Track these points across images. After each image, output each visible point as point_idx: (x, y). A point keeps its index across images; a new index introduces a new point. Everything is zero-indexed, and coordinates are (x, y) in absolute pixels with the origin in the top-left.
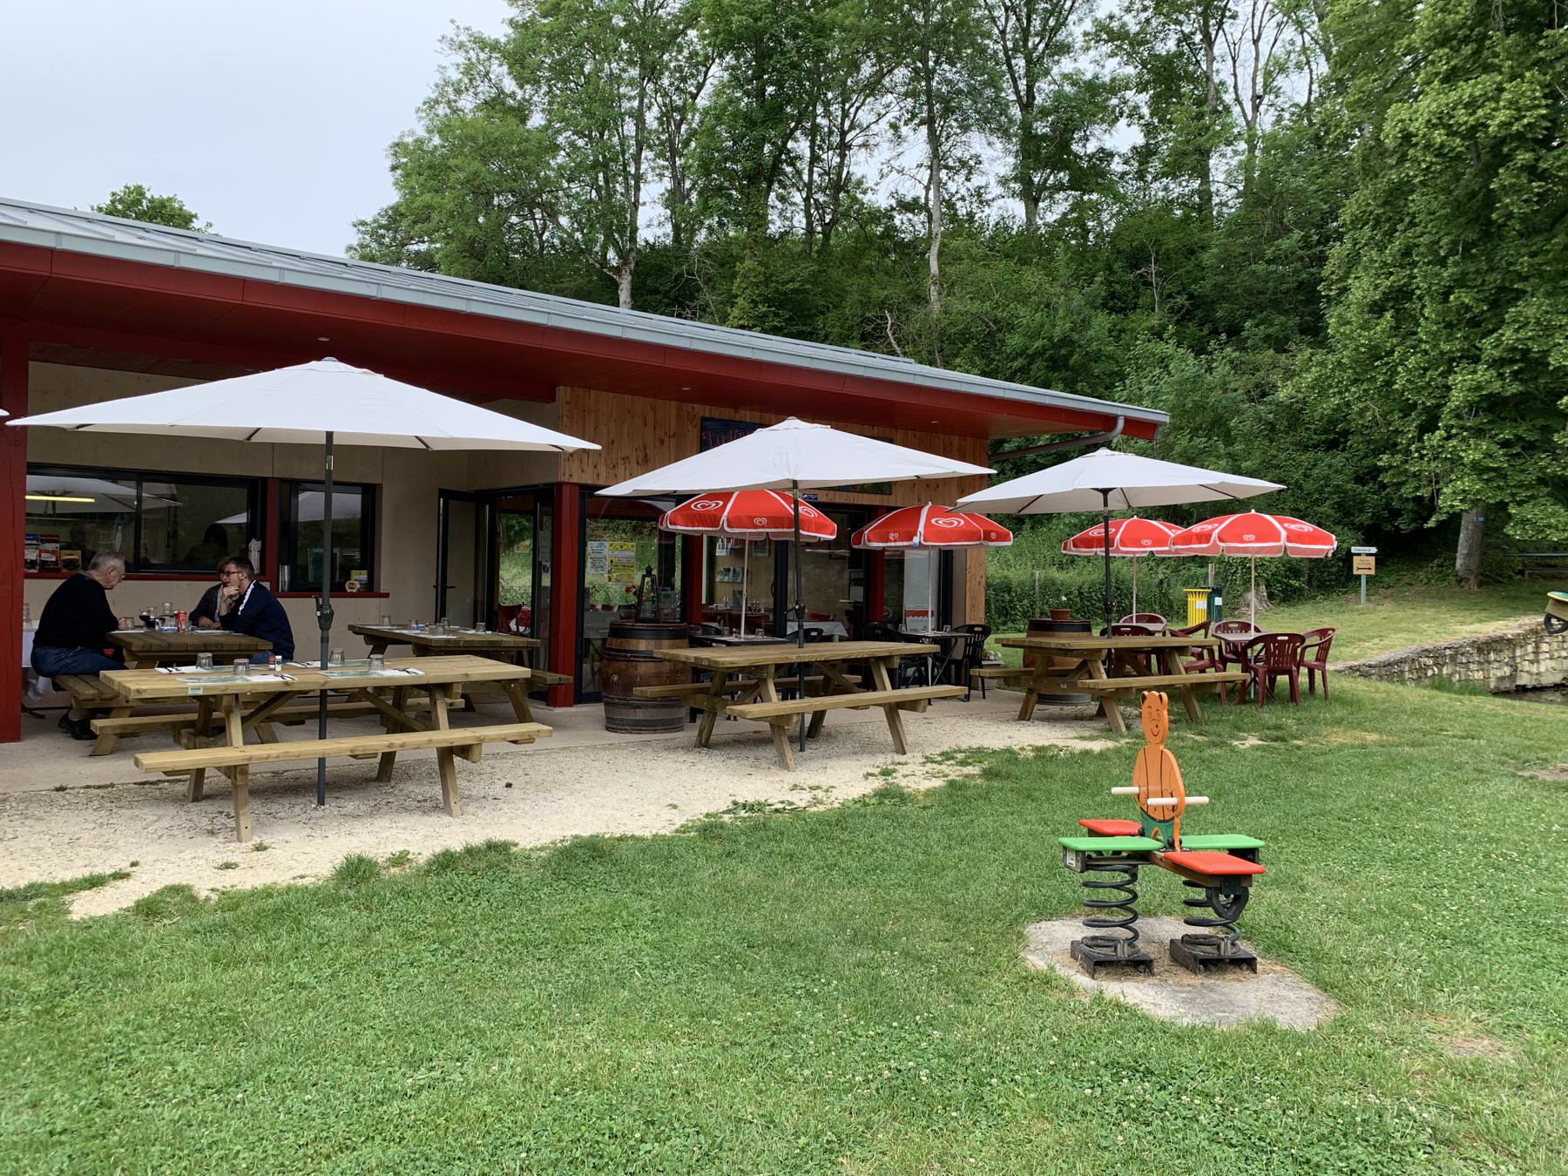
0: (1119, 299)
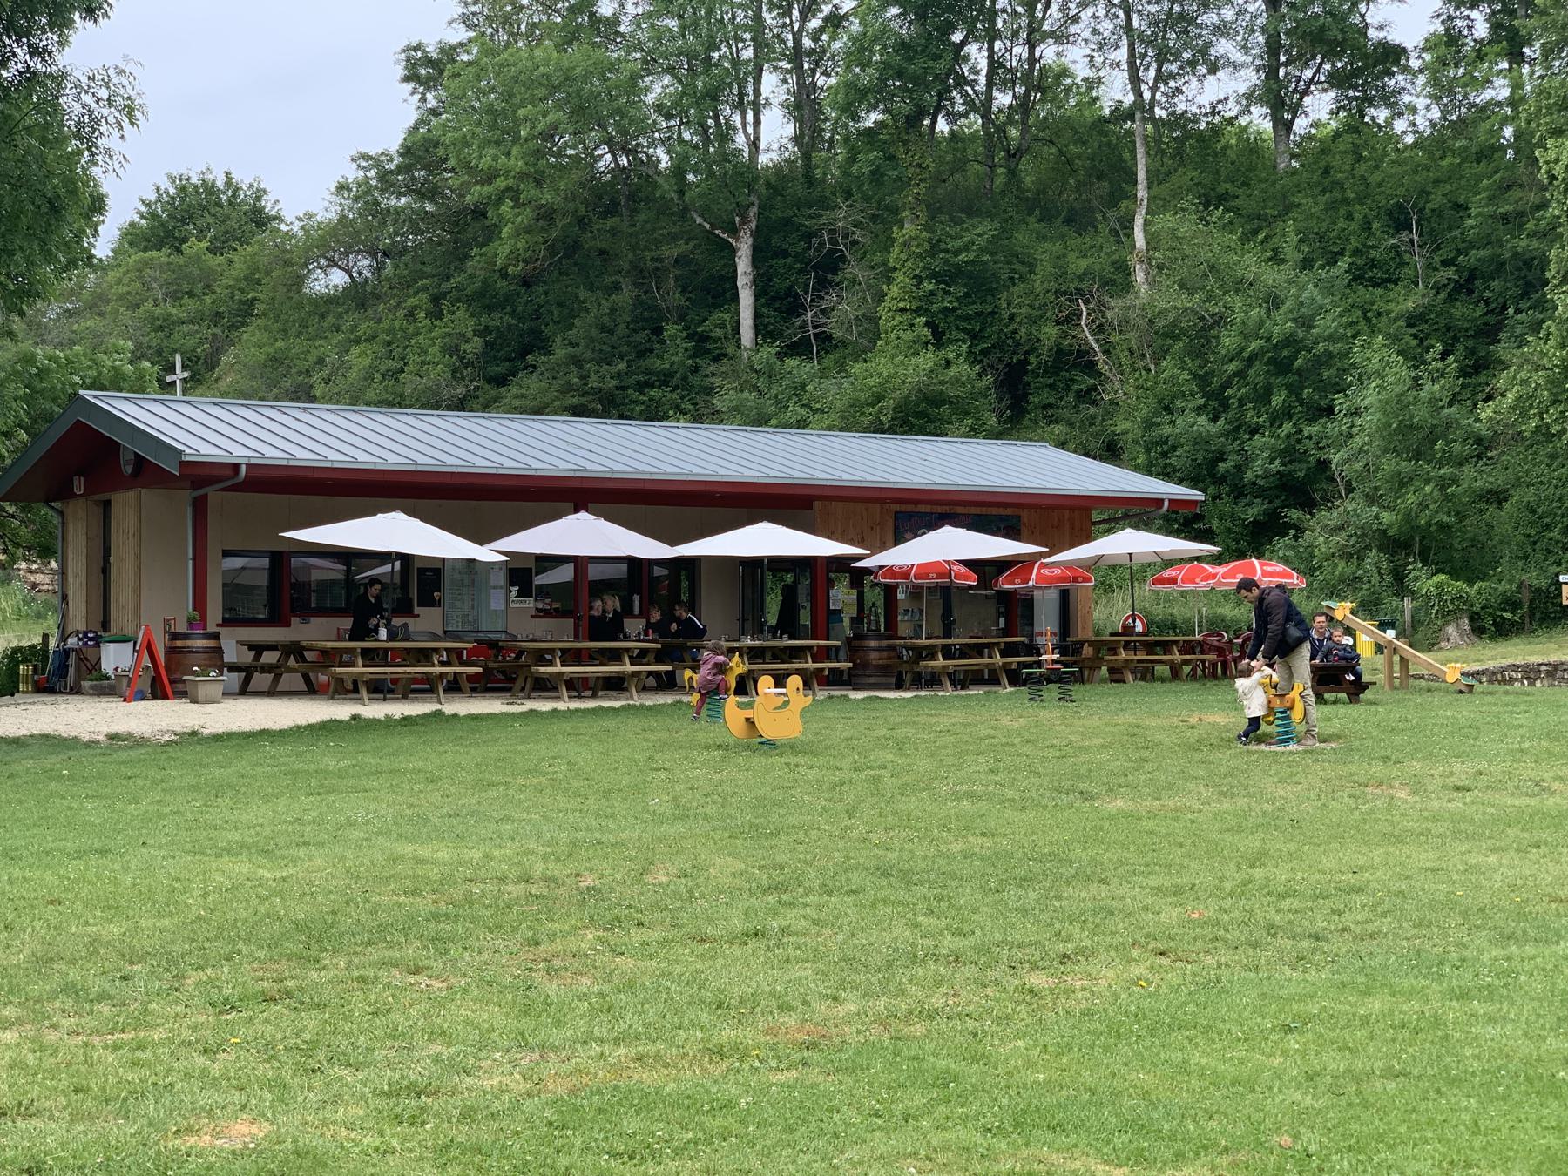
0: (1381, 268)
